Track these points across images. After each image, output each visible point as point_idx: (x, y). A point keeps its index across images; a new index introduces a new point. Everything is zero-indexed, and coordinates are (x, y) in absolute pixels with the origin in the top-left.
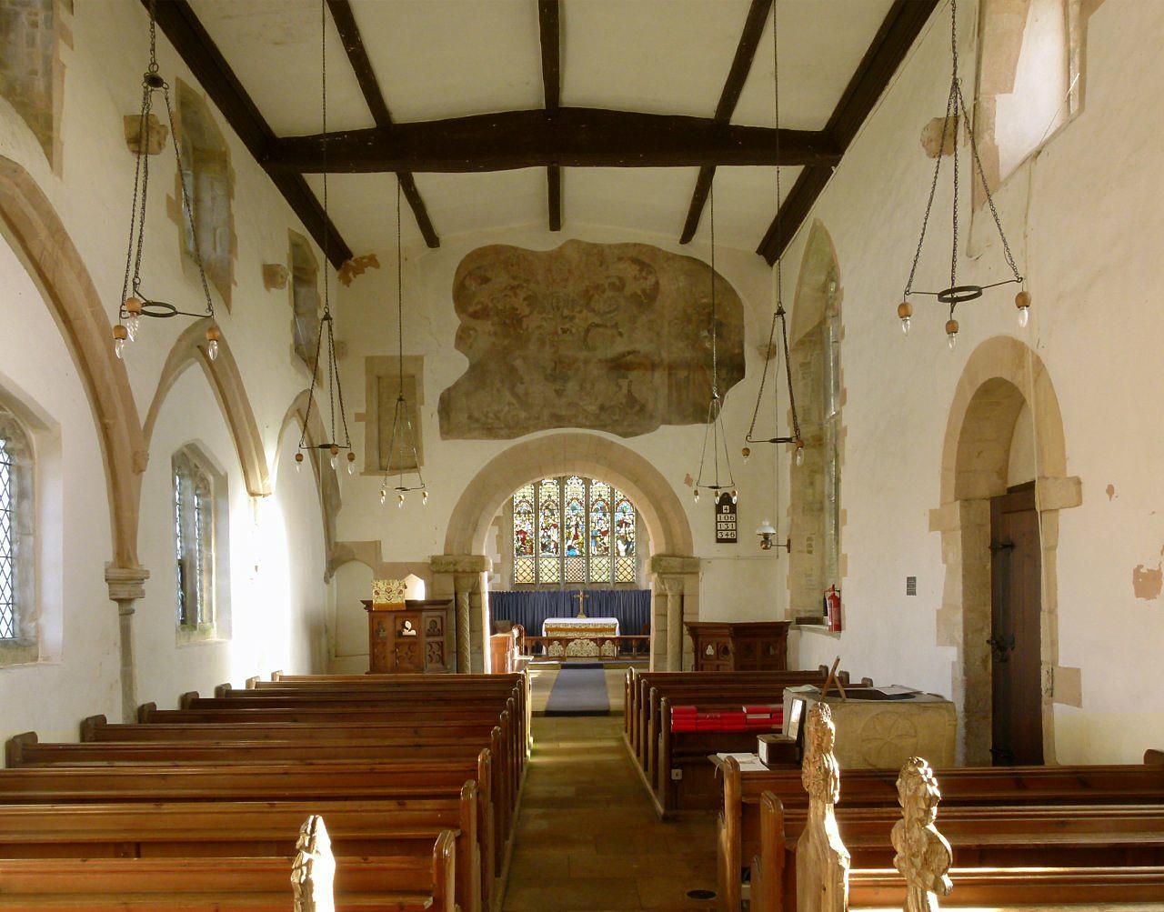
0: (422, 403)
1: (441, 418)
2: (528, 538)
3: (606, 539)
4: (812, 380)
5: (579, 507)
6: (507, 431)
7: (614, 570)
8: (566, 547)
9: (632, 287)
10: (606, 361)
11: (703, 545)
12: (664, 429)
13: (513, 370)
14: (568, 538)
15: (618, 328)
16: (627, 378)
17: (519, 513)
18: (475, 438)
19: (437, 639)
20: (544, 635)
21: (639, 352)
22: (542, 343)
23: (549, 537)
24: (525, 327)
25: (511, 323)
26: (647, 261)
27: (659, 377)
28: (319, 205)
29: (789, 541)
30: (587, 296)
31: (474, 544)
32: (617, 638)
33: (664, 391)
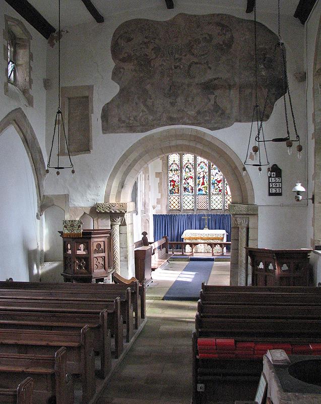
0: (92, 113)
1: (103, 121)
2: (176, 184)
3: (220, 185)
5: (205, 167)
6: (141, 127)
8: (197, 189)
11: (260, 195)
13: (145, 91)
14: (199, 184)
15: (208, 65)
17: (171, 170)
18: (122, 132)
19: (102, 255)
23: (188, 184)
24: (152, 65)
25: (144, 63)
29: (313, 196)
32: (225, 244)
33: (236, 103)
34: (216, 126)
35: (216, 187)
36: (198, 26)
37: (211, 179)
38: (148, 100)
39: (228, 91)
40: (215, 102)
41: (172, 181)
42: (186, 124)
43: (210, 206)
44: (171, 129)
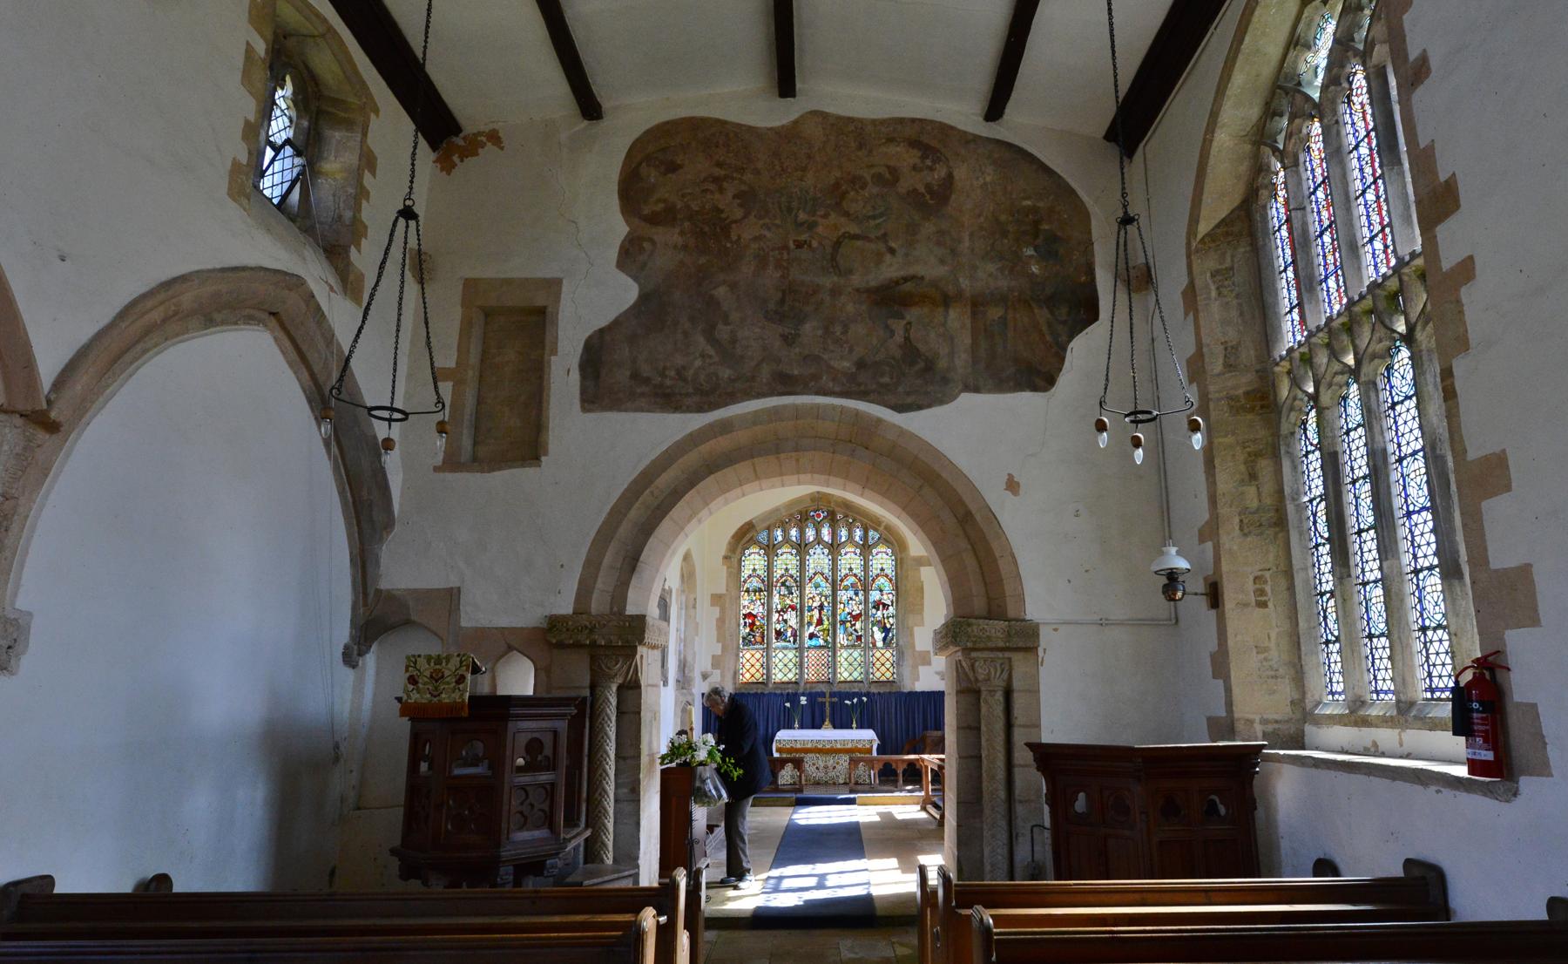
0: (554, 352)
1: (583, 377)
3: (858, 625)
4: (1237, 297)
5: (823, 584)
6: (696, 399)
7: (867, 665)
9: (908, 182)
10: (869, 291)
12: (966, 399)
13: (713, 303)
14: (810, 624)
15: (886, 242)
16: (903, 318)
17: (748, 591)
18: (642, 410)
19: (544, 777)
20: (776, 755)
21: (922, 278)
22: (762, 261)
24: (734, 238)
25: (711, 232)
26: (934, 143)
27: (957, 318)
28: (415, 57)
30: (837, 195)
31: (631, 594)
34: (909, 400)
36: (860, 147)
38: (720, 326)
39: (941, 309)
40: (907, 339)
41: (749, 615)
42: (825, 394)
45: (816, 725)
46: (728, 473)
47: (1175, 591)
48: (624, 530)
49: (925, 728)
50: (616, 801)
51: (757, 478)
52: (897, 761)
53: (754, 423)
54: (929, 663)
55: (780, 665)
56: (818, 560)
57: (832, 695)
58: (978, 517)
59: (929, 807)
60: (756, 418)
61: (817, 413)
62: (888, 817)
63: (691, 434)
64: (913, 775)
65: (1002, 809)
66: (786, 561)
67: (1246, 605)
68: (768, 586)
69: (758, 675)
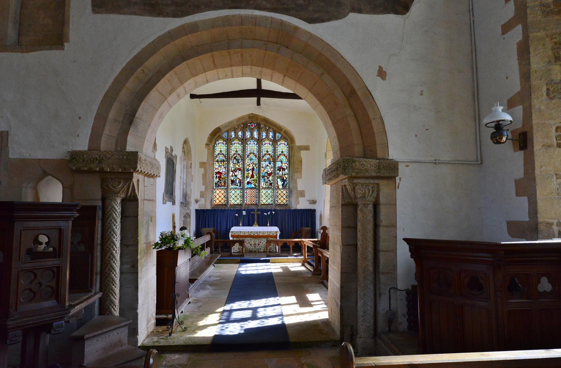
3: (271, 178)
5: (254, 158)
7: (275, 197)
8: (246, 182)
12: (353, 17)
14: (247, 177)
17: (218, 161)
18: (134, 13)
20: (231, 239)
31: (130, 139)
34: (316, 16)
35: (267, 180)
37: (262, 171)
41: (219, 173)
43: (259, 201)
44: (233, 16)
45: (250, 224)
46: (195, 61)
47: (501, 136)
48: (124, 95)
49: (302, 226)
50: (121, 273)
51: (216, 67)
52: (289, 242)
53: (213, 27)
54: (304, 196)
55: (233, 197)
56: (252, 147)
57: (258, 210)
58: (359, 94)
59: (306, 264)
60: (214, 23)
61: (255, 20)
62: (286, 269)
63: (169, 32)
64: (298, 248)
65: (371, 278)
66: (236, 147)
67: (550, 146)
68: (228, 158)
69: (222, 201)
